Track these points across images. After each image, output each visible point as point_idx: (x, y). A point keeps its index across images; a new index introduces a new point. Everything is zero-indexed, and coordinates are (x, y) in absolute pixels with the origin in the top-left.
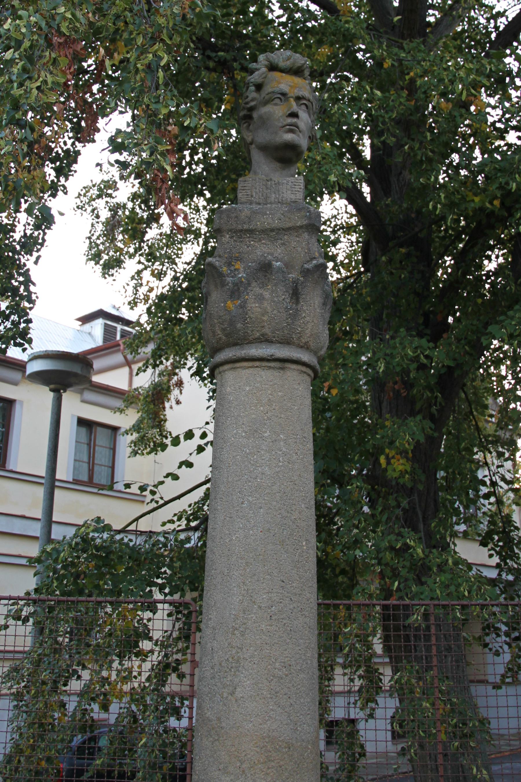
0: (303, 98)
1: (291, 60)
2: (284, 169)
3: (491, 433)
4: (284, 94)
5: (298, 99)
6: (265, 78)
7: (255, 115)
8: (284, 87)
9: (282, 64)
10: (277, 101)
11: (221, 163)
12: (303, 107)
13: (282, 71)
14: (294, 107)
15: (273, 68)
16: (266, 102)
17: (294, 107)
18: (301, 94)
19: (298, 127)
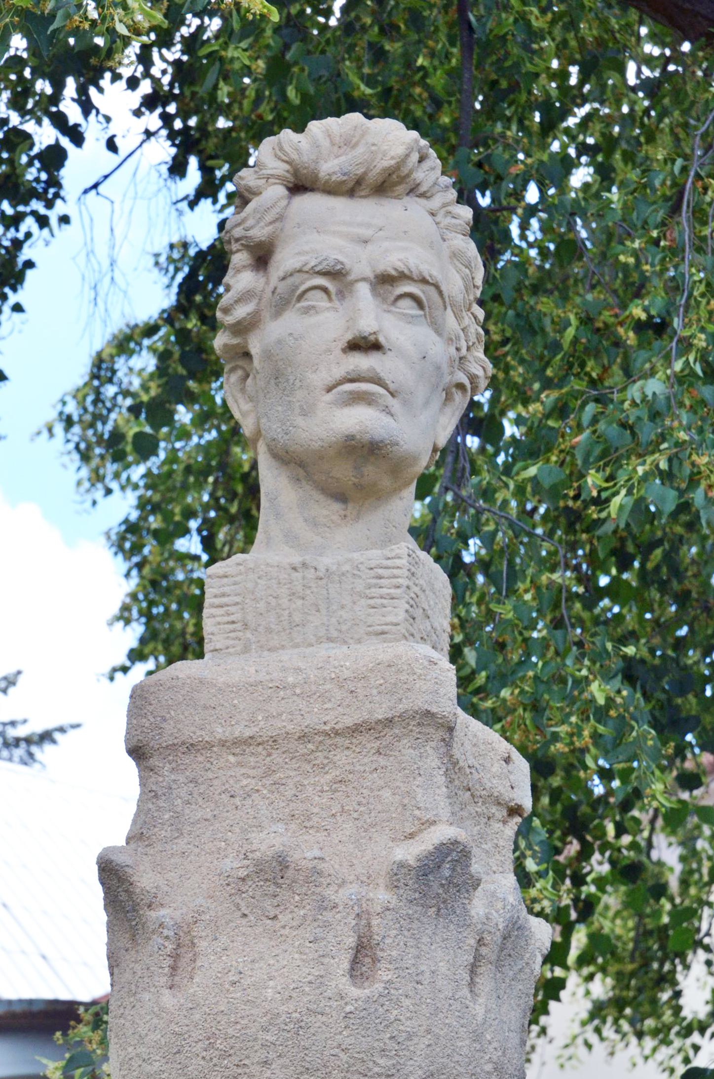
0: (403, 276)
1: (360, 150)
2: (357, 518)
3: (158, 559)
4: (336, 274)
5: (384, 281)
6: (280, 218)
7: (255, 347)
8: (329, 247)
9: (330, 167)
10: (317, 299)
11: (699, 637)
12: (407, 305)
13: (332, 189)
14: (368, 313)
15: (300, 185)
16: (282, 304)
17: (368, 313)
18: (392, 261)
19: (378, 381)
